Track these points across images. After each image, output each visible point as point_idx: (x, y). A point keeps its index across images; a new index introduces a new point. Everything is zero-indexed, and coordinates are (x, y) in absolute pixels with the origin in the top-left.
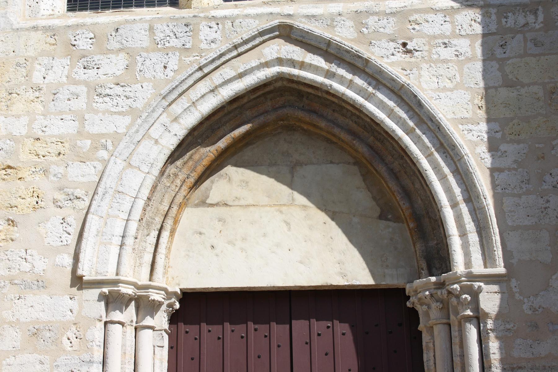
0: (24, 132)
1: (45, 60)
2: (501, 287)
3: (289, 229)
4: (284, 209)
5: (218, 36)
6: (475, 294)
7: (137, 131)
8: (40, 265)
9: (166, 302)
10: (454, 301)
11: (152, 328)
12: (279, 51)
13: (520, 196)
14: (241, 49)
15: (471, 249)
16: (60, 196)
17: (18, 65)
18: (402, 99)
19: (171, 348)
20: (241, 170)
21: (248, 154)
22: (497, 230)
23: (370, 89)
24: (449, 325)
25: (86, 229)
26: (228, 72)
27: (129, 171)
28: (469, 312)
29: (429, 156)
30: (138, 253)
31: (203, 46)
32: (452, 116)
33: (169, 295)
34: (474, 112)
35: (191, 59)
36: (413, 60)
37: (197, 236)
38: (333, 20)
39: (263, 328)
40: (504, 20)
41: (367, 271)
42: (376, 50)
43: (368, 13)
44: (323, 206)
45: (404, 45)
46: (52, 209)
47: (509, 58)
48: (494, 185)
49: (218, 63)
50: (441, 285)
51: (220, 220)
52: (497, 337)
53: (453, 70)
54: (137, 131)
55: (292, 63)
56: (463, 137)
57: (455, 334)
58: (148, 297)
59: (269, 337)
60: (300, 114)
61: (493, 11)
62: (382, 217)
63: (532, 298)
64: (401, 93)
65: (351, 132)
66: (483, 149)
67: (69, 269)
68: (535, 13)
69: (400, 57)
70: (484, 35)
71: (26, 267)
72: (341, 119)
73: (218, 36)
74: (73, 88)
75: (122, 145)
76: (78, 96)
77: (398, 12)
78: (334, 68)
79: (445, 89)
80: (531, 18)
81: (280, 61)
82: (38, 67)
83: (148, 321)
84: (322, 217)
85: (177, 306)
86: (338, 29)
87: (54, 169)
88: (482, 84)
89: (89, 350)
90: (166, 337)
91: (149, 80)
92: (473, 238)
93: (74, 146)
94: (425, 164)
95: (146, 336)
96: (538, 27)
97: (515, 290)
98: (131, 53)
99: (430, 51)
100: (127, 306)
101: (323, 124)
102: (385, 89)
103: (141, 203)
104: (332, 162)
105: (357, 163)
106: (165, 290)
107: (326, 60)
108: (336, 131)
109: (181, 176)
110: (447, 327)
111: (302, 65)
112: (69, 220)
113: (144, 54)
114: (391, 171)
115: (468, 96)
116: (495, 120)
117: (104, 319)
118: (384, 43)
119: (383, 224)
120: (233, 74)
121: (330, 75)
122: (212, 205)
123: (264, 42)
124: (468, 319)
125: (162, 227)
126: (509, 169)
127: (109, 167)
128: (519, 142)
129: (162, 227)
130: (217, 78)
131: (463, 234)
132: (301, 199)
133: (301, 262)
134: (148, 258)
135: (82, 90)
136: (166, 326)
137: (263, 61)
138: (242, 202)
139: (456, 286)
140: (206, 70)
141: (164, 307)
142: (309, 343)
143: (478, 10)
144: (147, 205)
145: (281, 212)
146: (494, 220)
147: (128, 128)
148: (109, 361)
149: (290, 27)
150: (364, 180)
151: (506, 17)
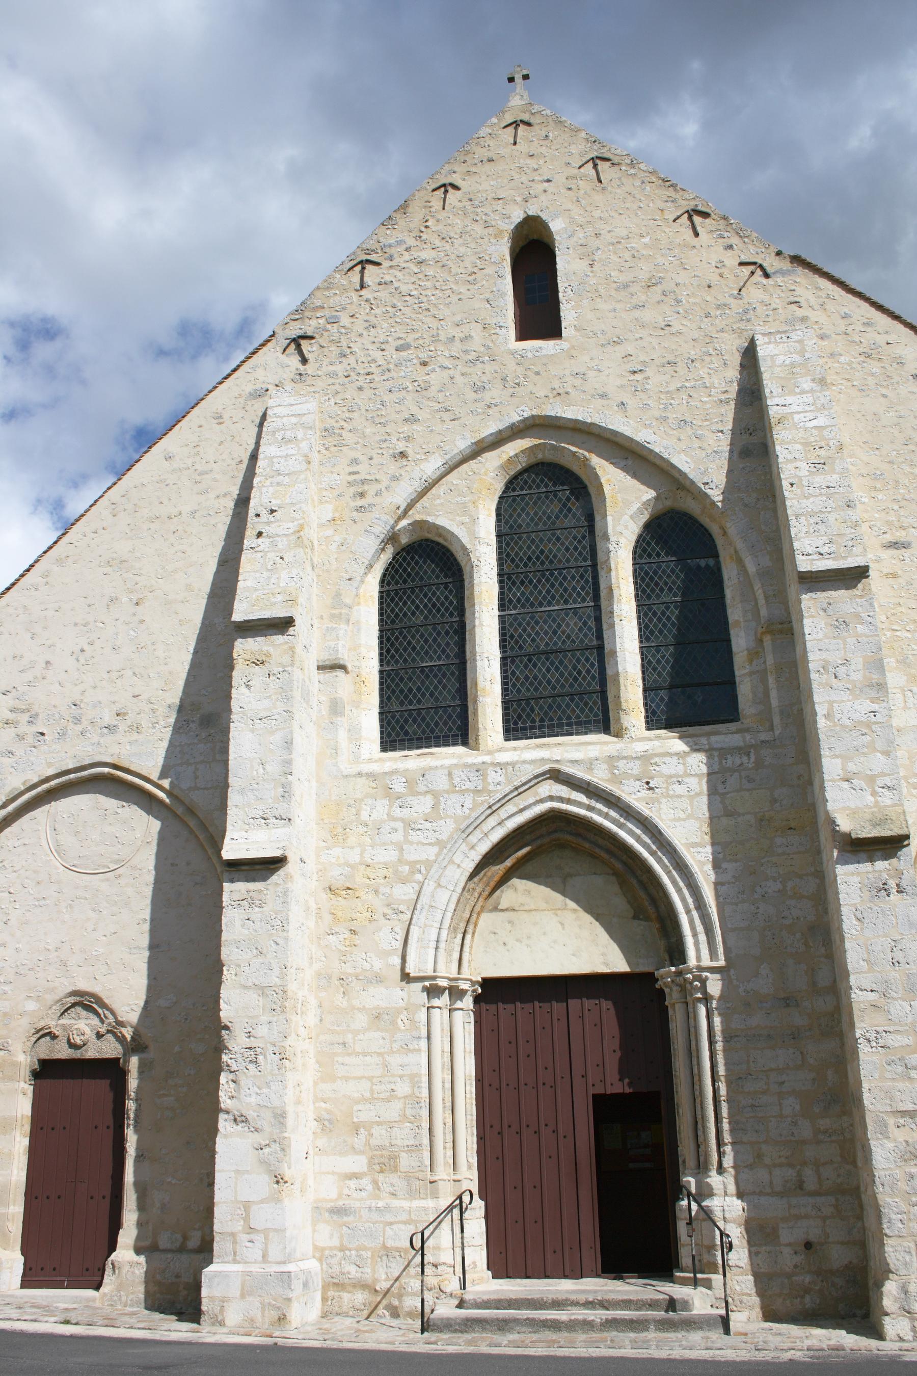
0: (358, 860)
1: (370, 801)
2: (722, 976)
3: (564, 928)
4: (559, 912)
5: (502, 779)
6: (704, 981)
7: (444, 859)
8: (378, 964)
9: (471, 989)
10: (688, 986)
11: (462, 1009)
12: (550, 791)
13: (736, 904)
14: (521, 790)
15: (701, 946)
16: (389, 911)
17: (349, 805)
18: (647, 828)
19: (476, 1022)
20: (524, 881)
21: (529, 867)
22: (719, 932)
23: (622, 820)
24: (687, 1003)
25: (410, 934)
26: (511, 808)
27: (439, 890)
28: (699, 995)
29: (668, 873)
30: (449, 953)
31: (491, 788)
32: (685, 841)
33: (473, 983)
34: (702, 838)
35: (483, 798)
36: (654, 795)
37: (492, 935)
38: (591, 764)
39: (546, 1006)
40: (724, 761)
41: (624, 960)
42: (625, 788)
43: (619, 758)
44: (589, 910)
45: (648, 783)
46: (383, 921)
47: (727, 793)
48: (717, 896)
49: (503, 801)
50: (679, 973)
51: (509, 922)
52: (720, 1014)
53: (686, 803)
54: (444, 859)
55: (561, 799)
56: (693, 858)
57: (691, 1010)
58: (458, 987)
59: (551, 1013)
60: (569, 838)
61: (716, 754)
62: (635, 917)
63: (746, 984)
64: (646, 823)
65: (608, 851)
66: (709, 867)
67: (399, 967)
68: (748, 754)
69: (645, 793)
70: (709, 774)
71: (367, 966)
72: (600, 841)
73: (502, 779)
74: (393, 824)
75: (433, 871)
76: (397, 831)
77: (642, 756)
78: (593, 803)
79: (679, 819)
80: (745, 759)
81: (551, 798)
82: (365, 807)
83: (459, 1004)
84: (588, 918)
85: (480, 991)
86: (595, 771)
87: (382, 889)
88: (707, 815)
89: (418, 1028)
90: (472, 1014)
91: (451, 817)
92: (702, 937)
93: (397, 871)
94: (665, 880)
95: (458, 1015)
96: (750, 766)
97: (733, 977)
98: (436, 795)
99: (667, 788)
100: (443, 993)
101: (587, 845)
102: (633, 820)
103: (449, 915)
104: (595, 874)
105: (616, 874)
106: (470, 980)
107: (587, 797)
108: (597, 850)
109: (478, 890)
110: (685, 1005)
111: (569, 801)
112: (397, 929)
113: (445, 795)
114: (641, 883)
115: (697, 825)
116: (718, 844)
117: (427, 1005)
118: (631, 782)
119: (636, 923)
120: (515, 809)
121: (590, 808)
122: (503, 910)
123: (538, 783)
124: (699, 1000)
125: (465, 931)
126: (729, 883)
127: (424, 888)
128: (736, 861)
129: (465, 931)
130: (503, 813)
131: (695, 935)
132: (572, 904)
133: (573, 955)
134: (456, 956)
135: (399, 825)
136: (471, 1006)
137: (538, 798)
138: (526, 908)
139: (689, 976)
140: (494, 808)
141: (469, 993)
142: (582, 1017)
143: (704, 754)
144: (454, 915)
145: (557, 915)
146: (717, 924)
147: (437, 855)
148: (433, 1036)
149: (559, 771)
150: (621, 888)
151: (726, 759)
